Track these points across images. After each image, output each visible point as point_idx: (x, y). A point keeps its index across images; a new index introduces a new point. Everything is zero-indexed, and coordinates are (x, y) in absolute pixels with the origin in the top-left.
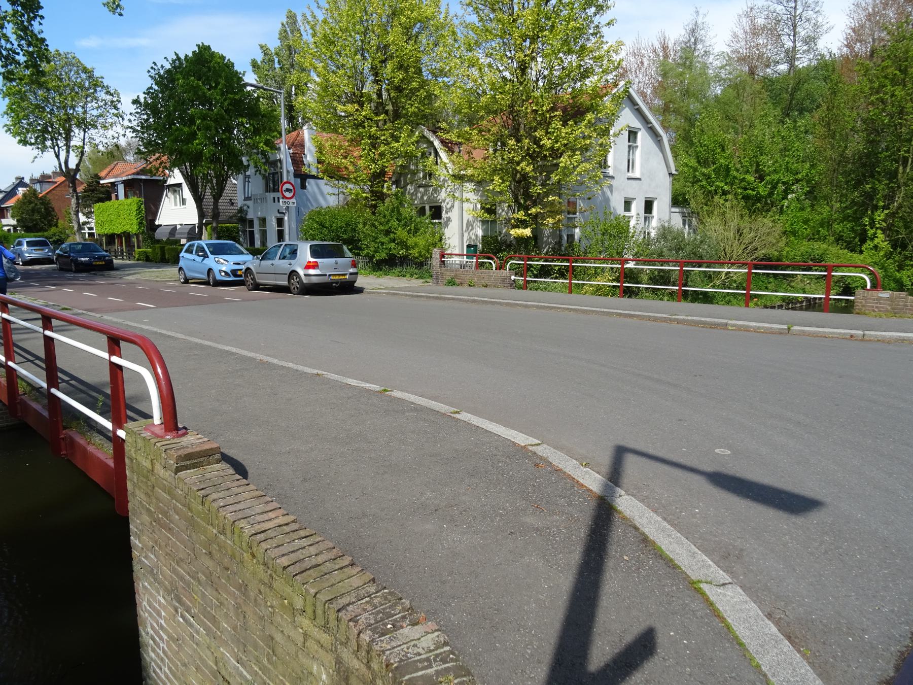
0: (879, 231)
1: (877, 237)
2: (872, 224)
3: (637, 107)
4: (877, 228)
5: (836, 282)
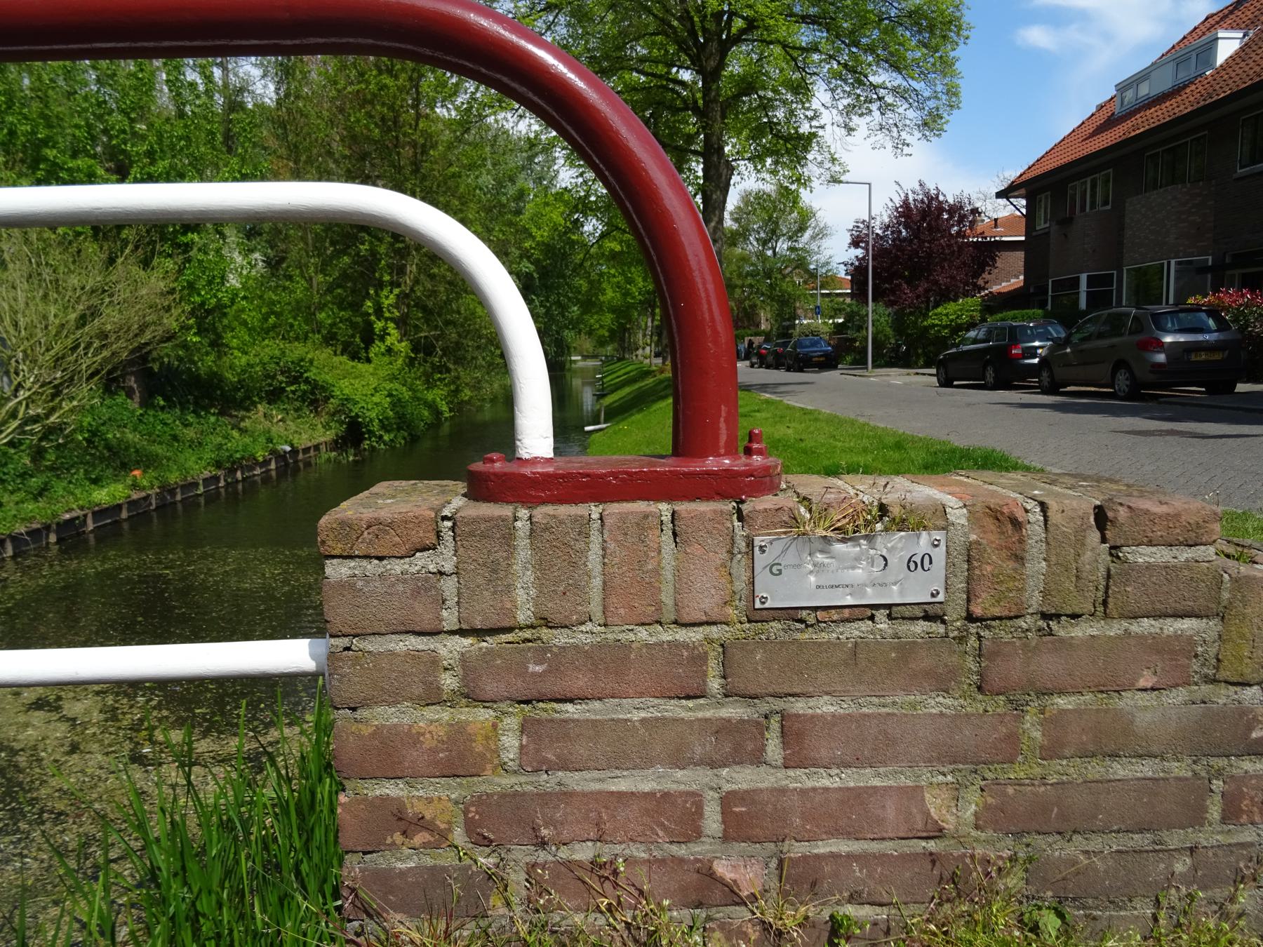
0: (391, 325)
1: (389, 334)
2: (379, 312)
5: (333, 415)
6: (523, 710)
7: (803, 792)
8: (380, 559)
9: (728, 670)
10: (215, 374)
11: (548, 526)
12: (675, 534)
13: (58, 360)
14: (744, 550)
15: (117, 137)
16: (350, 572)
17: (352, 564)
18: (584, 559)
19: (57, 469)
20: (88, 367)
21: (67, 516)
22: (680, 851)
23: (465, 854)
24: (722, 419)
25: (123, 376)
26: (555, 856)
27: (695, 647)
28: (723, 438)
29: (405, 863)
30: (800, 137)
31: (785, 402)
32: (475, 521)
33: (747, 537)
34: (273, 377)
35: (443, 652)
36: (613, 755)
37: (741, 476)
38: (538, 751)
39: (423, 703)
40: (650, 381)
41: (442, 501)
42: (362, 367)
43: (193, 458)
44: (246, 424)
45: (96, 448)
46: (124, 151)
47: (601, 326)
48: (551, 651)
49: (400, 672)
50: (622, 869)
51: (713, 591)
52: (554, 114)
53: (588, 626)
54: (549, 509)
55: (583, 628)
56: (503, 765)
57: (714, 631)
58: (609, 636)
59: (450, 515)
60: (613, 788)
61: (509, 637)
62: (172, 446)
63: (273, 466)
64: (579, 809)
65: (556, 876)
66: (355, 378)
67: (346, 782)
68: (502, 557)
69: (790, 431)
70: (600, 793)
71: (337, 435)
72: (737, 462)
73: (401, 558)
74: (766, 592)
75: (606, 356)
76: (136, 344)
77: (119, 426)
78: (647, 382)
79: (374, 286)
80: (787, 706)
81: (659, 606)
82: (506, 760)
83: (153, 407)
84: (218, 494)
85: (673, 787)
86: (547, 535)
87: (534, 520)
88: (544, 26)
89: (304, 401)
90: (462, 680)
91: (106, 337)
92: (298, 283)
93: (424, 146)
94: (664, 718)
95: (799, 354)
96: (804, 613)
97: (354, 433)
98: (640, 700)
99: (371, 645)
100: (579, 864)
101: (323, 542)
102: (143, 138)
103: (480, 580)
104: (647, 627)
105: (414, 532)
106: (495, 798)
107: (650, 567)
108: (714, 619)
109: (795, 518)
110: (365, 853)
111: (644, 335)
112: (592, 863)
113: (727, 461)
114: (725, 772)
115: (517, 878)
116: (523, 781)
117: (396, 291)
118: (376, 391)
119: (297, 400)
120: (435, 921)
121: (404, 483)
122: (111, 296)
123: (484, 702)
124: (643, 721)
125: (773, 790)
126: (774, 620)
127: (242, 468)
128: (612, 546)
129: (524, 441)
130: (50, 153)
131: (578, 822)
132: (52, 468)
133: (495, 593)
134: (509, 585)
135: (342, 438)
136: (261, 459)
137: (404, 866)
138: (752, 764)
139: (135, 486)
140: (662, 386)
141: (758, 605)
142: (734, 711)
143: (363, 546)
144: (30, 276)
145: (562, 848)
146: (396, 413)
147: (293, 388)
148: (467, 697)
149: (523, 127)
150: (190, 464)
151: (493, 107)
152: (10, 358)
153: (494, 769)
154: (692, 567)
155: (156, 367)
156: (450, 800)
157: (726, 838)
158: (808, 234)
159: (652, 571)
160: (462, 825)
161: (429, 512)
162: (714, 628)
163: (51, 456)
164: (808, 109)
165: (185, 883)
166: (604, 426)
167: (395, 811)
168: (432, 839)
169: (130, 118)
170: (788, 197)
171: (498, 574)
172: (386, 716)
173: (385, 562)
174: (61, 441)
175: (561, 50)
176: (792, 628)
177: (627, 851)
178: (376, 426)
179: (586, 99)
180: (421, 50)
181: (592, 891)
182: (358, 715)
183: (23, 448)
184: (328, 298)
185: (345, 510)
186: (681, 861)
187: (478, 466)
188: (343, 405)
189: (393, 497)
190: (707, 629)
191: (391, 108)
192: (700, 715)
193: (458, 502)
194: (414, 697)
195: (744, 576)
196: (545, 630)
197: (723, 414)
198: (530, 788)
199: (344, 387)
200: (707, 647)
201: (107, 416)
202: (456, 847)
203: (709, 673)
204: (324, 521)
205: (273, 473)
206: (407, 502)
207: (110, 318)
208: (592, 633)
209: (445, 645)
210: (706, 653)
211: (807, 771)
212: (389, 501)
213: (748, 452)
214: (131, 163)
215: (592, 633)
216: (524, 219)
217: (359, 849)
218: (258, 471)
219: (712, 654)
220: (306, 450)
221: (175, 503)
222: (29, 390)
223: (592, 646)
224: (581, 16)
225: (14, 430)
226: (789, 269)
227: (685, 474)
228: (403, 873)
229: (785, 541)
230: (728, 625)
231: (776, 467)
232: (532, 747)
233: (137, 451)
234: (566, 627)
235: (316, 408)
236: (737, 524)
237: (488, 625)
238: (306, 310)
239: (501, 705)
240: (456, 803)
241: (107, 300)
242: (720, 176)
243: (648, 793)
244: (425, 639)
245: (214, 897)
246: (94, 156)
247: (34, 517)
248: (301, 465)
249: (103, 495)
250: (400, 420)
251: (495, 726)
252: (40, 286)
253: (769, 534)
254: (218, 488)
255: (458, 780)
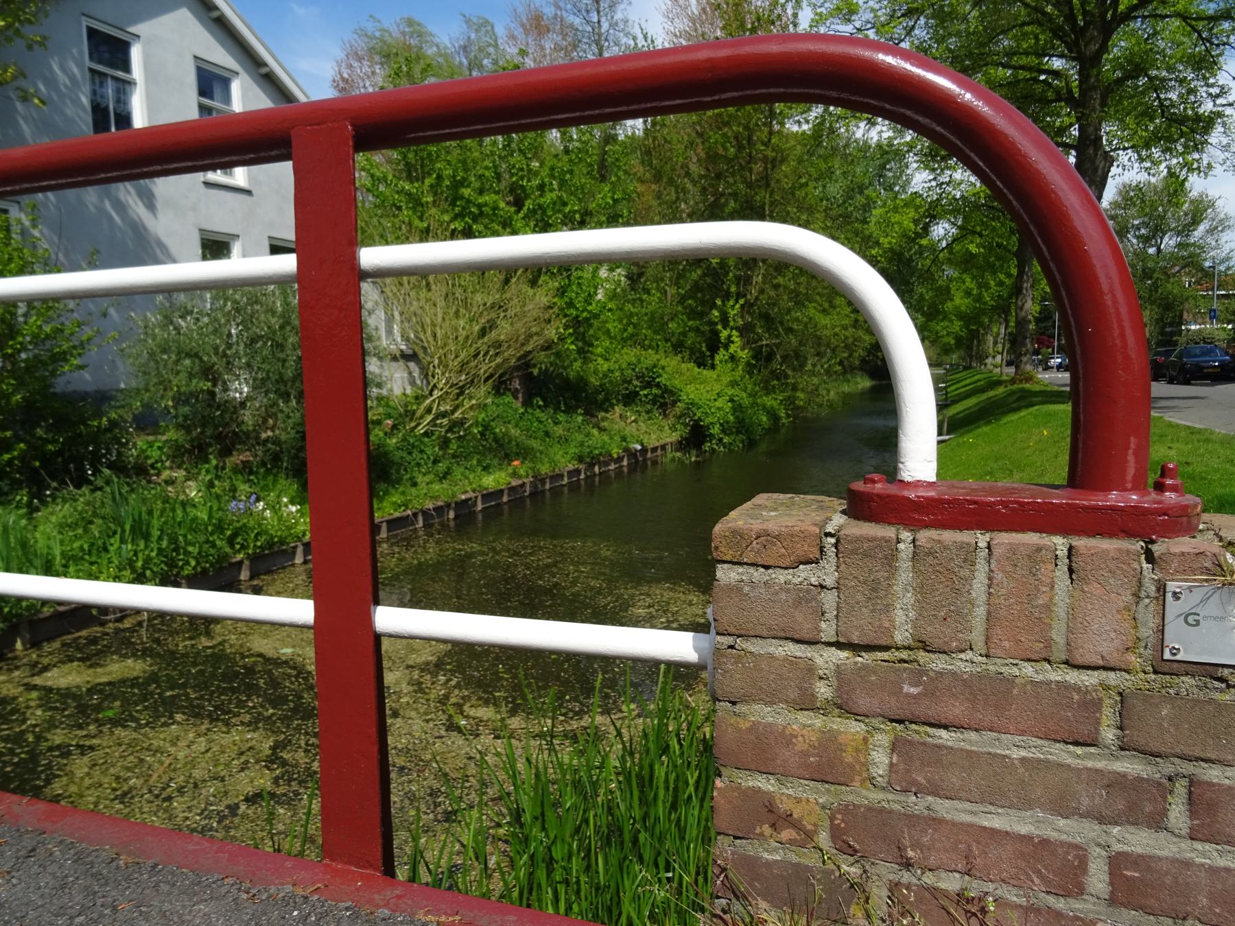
0: (734, 332)
1: (733, 342)
2: (725, 321)
3: (215, 14)
4: (732, 329)
5: (679, 418)
6: (894, 729)
7: (1213, 870)
8: (767, 567)
9: (1126, 722)
10: (582, 377)
11: (932, 551)
12: (1071, 571)
13: (463, 365)
14: (1153, 594)
15: (517, 174)
16: (737, 577)
17: (741, 570)
18: (968, 586)
19: (458, 457)
20: (485, 372)
21: (463, 497)
22: (1060, 904)
23: (829, 858)
24: (1131, 452)
25: (510, 380)
26: (919, 879)
27: (1087, 692)
28: (1131, 471)
29: (771, 854)
30: (1198, 118)
31: (1167, 418)
32: (858, 539)
33: (1159, 580)
34: (630, 382)
35: (819, 661)
36: (988, 789)
37: (1152, 514)
38: (908, 771)
39: (798, 707)
40: (1001, 390)
41: (823, 518)
42: (707, 373)
43: (561, 453)
44: (605, 424)
45: (486, 440)
46: (522, 186)
47: (948, 334)
48: (927, 675)
49: (778, 674)
50: (992, 908)
51: (1113, 635)
52: (958, 142)
53: (969, 655)
54: (933, 533)
55: (962, 656)
56: (871, 779)
57: (1112, 678)
58: (991, 668)
59: (833, 532)
60: (986, 824)
61: (885, 655)
62: (545, 441)
63: (625, 463)
64: (948, 838)
65: (920, 899)
66: (701, 383)
67: (722, 769)
68: (883, 577)
69: (1172, 453)
70: (971, 825)
71: (681, 437)
72: (1146, 499)
73: (786, 568)
74: (1179, 642)
75: (951, 365)
76: (522, 352)
77: (505, 422)
78: (997, 393)
79: (721, 297)
80: (1197, 771)
81: (1048, 644)
82: (875, 775)
83: (531, 406)
84: (579, 486)
85: (1053, 835)
86: (930, 559)
87: (918, 543)
88: (904, 32)
89: (654, 404)
90: (836, 691)
91: (500, 346)
92: (654, 295)
93: (774, 160)
94: (1047, 761)
95: (1186, 364)
96: (1226, 672)
97: (696, 436)
98: (1020, 738)
99: (754, 646)
100: (945, 894)
101: (716, 548)
102: (536, 174)
103: (859, 597)
104: (1033, 664)
105: (799, 546)
106: (862, 810)
107: (1040, 602)
108: (1112, 664)
109: (1220, 566)
110: (736, 838)
111: (995, 343)
112: (958, 895)
113: (1135, 497)
114: (1116, 830)
115: (879, 893)
116: (890, 798)
117: (742, 301)
118: (719, 397)
119: (648, 403)
120: (796, 916)
121: (782, 496)
122: (506, 311)
123: (857, 715)
124: (1023, 760)
125: (1174, 861)
126: (1187, 674)
127: (599, 463)
128: (999, 576)
129: (907, 464)
130: (466, 192)
131: (946, 851)
132: (454, 456)
133: (874, 611)
134: (888, 605)
135: (686, 439)
136: (615, 456)
137: (770, 857)
138: (1150, 827)
139: (515, 474)
140: (1015, 397)
141: (1167, 656)
142: (1130, 766)
143: (752, 555)
144: (447, 295)
145: (928, 873)
146: (737, 418)
147: (645, 392)
148: (840, 707)
149: (873, 136)
150: (558, 457)
151: (847, 118)
152: (429, 363)
153: (863, 782)
154: (1089, 607)
155: (536, 372)
156: (817, 803)
157: (1113, 901)
158: (1202, 228)
159: (1042, 606)
160: (828, 830)
161: (815, 528)
162: (1112, 675)
163: (454, 446)
164: (1212, 86)
165: (544, 829)
166: (947, 437)
167: (767, 804)
168: (798, 838)
169: (526, 158)
170: (1175, 187)
171: (878, 593)
172: (762, 714)
173: (770, 571)
174: (462, 433)
175: (921, 55)
176: (1209, 685)
177: (999, 892)
178: (716, 430)
179: (993, 124)
180: (828, 93)
181: (956, 923)
182: (737, 708)
183: (434, 438)
184: (680, 308)
185: (735, 520)
186: (1059, 914)
187: (859, 486)
188: (688, 408)
189: (775, 510)
190: (1104, 674)
191: (746, 128)
192: (1090, 764)
193: (837, 521)
194: (789, 700)
195: (1152, 622)
196: (922, 653)
197: (1133, 446)
198: (896, 807)
199: (690, 392)
200: (1102, 694)
201: (497, 413)
202: (821, 850)
203: (1103, 721)
204: (718, 528)
205: (625, 470)
206: (790, 515)
207: (504, 330)
208: (972, 663)
209: (821, 655)
210: (1100, 699)
211: (1219, 847)
212: (773, 514)
213: (1160, 487)
214: (527, 196)
215: (972, 663)
216: (872, 228)
217: (731, 833)
218: (612, 467)
219: (1107, 701)
220: (654, 449)
221: (543, 492)
222: (442, 389)
223: (972, 674)
224: (943, 17)
225: (428, 424)
226: (1177, 268)
227: (1084, 508)
228: (769, 864)
229: (1206, 590)
230: (1129, 673)
231: (1196, 506)
232: (902, 766)
233: (517, 445)
234: (945, 652)
235: (665, 411)
236: (1145, 565)
237: (865, 641)
238: (658, 323)
239: (873, 720)
240: (824, 807)
241: (502, 315)
242: (1096, 170)
243: (1024, 836)
244: (803, 647)
245: (566, 847)
246: (497, 193)
247: (439, 496)
248: (649, 463)
249: (490, 481)
250: (741, 425)
251: (865, 740)
252: (453, 303)
253: (1186, 580)
254: (579, 480)
255: (827, 786)
